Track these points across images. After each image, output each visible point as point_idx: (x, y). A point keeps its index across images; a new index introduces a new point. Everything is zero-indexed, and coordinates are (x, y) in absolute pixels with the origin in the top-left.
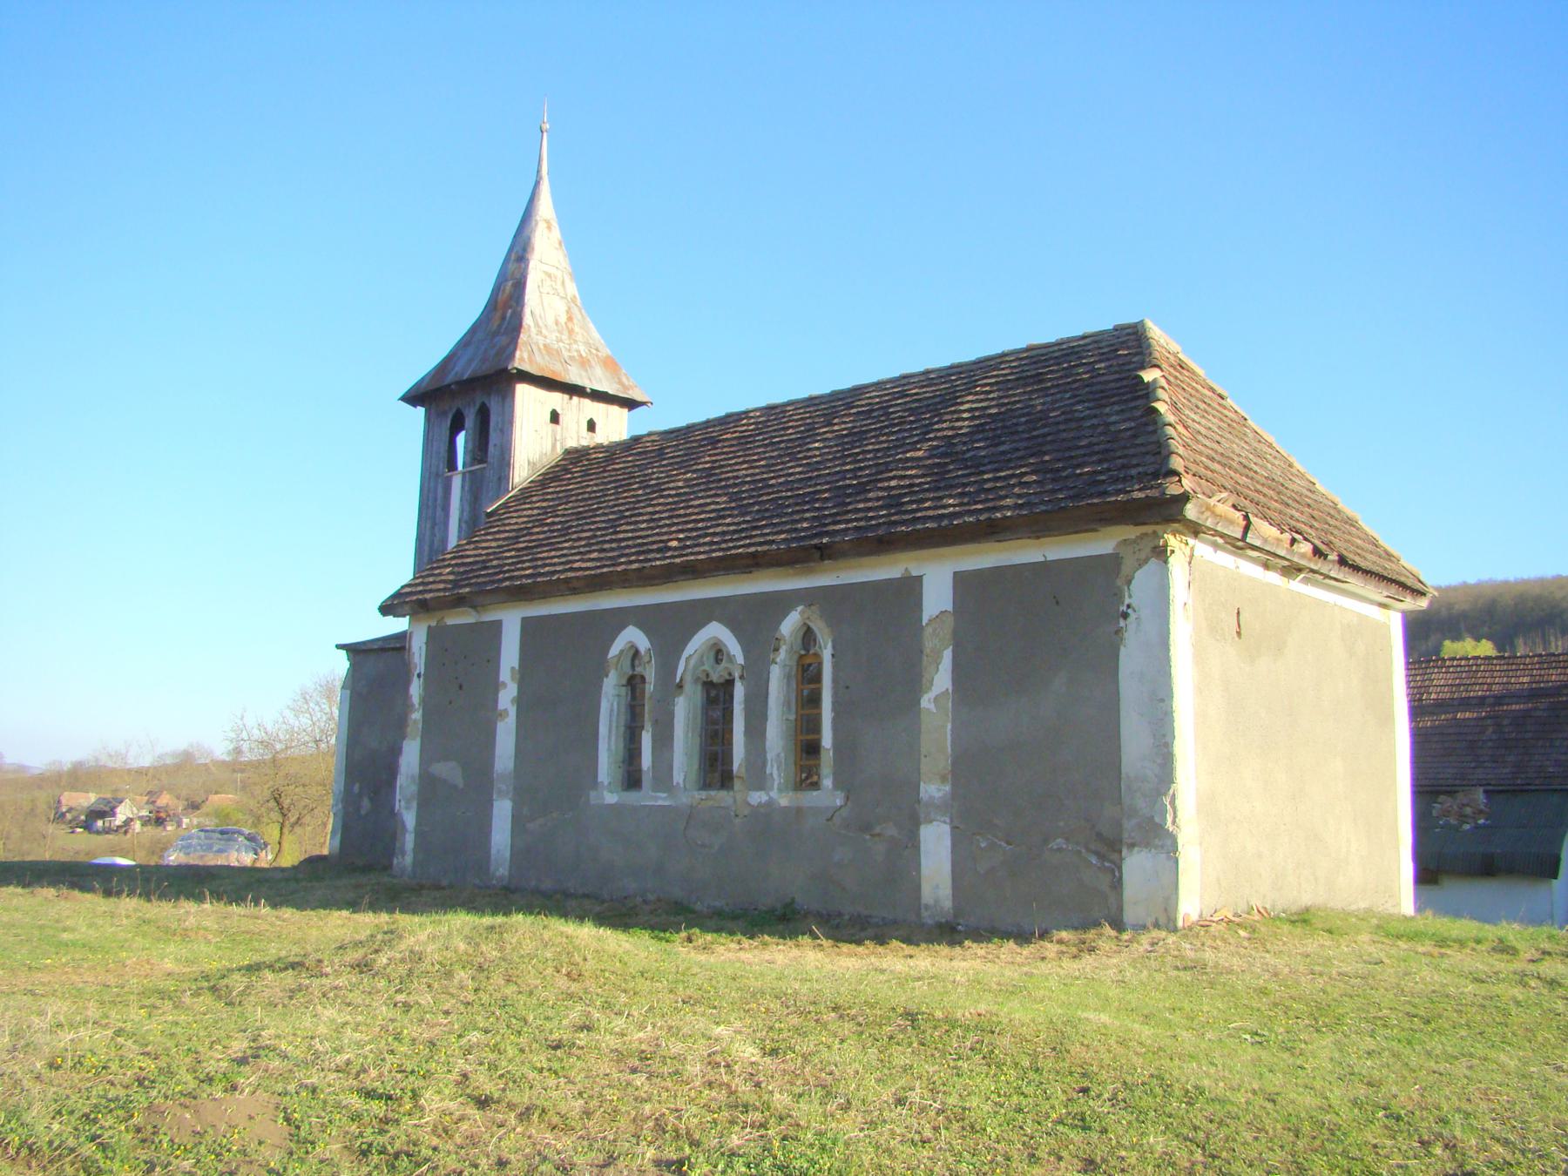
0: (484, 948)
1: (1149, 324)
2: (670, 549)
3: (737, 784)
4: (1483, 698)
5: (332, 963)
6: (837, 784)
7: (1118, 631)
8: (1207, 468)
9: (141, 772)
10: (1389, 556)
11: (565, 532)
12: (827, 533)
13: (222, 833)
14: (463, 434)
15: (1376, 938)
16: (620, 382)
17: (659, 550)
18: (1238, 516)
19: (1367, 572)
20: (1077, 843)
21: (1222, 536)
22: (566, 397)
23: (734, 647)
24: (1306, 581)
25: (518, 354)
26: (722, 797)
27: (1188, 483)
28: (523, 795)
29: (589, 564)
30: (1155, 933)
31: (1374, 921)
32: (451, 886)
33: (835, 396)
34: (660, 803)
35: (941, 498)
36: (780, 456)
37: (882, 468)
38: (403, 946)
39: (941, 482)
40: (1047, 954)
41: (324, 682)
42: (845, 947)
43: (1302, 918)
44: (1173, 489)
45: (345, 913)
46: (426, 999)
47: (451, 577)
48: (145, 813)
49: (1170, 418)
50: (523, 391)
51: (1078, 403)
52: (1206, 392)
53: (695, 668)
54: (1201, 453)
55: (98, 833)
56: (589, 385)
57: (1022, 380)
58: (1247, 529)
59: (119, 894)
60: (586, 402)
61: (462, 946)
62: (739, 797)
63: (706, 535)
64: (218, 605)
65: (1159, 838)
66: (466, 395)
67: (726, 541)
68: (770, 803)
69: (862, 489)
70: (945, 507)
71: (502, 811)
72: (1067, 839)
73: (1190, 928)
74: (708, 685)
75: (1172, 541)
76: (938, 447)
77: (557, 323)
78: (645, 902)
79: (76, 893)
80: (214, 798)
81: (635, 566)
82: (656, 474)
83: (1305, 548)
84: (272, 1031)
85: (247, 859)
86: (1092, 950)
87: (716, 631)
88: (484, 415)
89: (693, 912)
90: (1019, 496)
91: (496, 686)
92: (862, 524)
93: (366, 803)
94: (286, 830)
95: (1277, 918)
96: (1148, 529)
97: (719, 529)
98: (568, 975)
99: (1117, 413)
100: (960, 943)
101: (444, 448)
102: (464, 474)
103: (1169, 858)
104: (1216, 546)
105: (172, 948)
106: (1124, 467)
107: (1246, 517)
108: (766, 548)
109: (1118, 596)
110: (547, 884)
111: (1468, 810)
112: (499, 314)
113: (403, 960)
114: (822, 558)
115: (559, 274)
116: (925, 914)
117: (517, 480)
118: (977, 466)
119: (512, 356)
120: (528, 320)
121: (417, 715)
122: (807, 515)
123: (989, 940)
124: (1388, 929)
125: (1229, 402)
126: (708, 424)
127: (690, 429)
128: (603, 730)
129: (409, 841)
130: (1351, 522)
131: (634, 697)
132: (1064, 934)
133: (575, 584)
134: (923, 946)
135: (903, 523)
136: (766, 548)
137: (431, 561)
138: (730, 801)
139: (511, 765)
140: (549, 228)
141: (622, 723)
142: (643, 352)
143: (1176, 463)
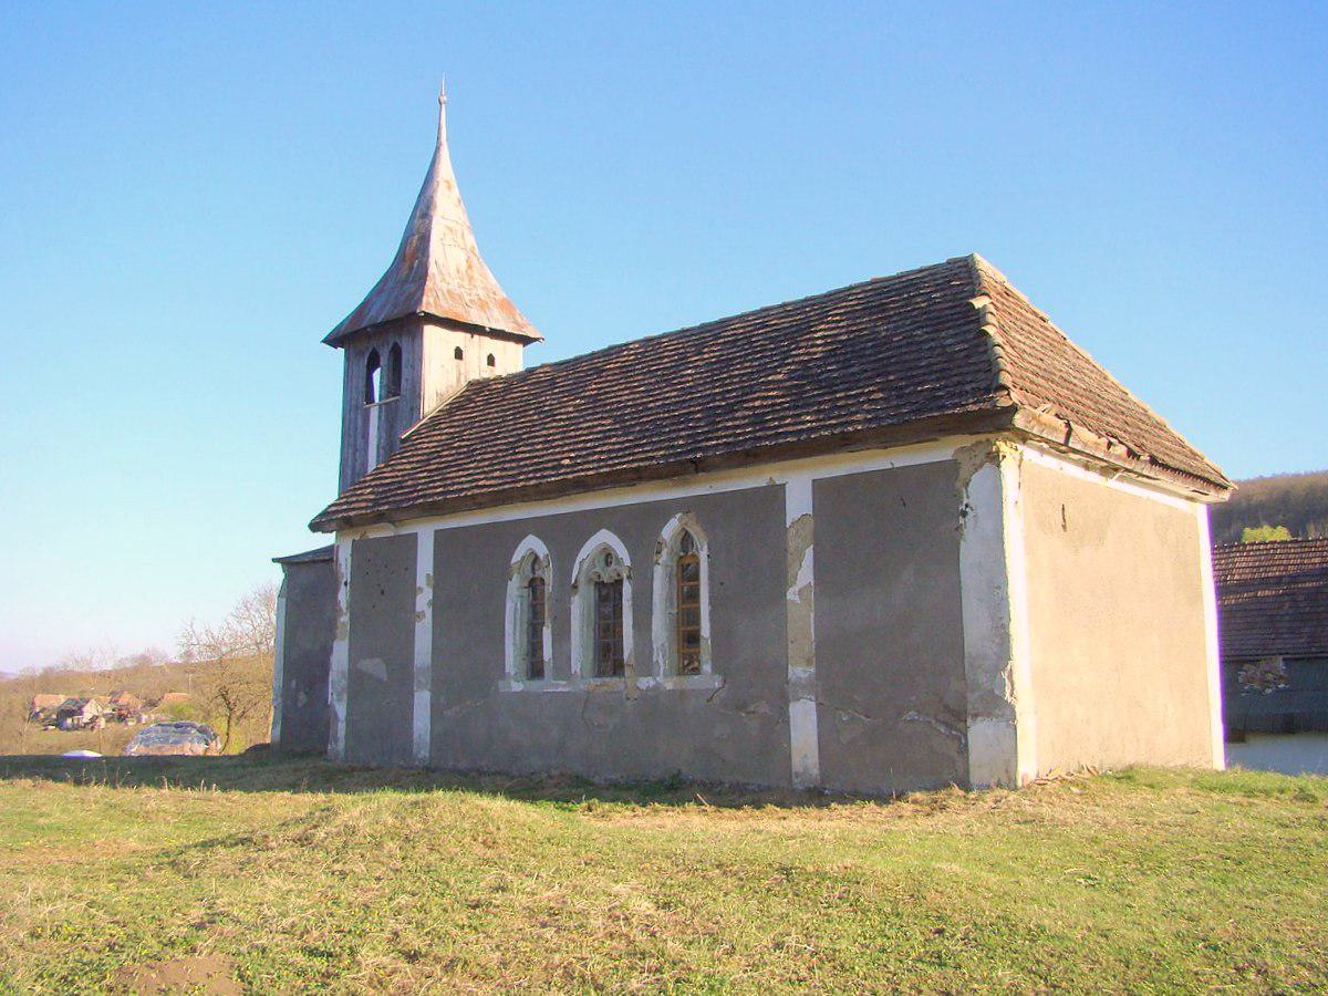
0: (409, 821)
1: (978, 257)
2: (563, 466)
3: (627, 671)
4: (1281, 577)
5: (277, 838)
6: (715, 670)
7: (959, 528)
8: (1032, 382)
9: (104, 675)
10: (1194, 455)
11: (470, 454)
12: (700, 449)
13: (177, 726)
14: (379, 369)
15: (1192, 791)
16: (516, 322)
17: (553, 468)
18: (1061, 423)
19: (1175, 470)
20: (927, 715)
21: (1047, 441)
22: (469, 335)
23: (622, 552)
24: (1121, 479)
25: (425, 299)
26: (614, 683)
27: (1016, 396)
28: (439, 685)
29: (493, 482)
30: (998, 792)
31: (1190, 776)
32: (379, 768)
33: (704, 328)
34: (560, 690)
35: (799, 415)
36: (658, 382)
37: (747, 390)
38: (338, 822)
39: (799, 402)
40: (903, 813)
41: (262, 592)
42: (727, 812)
43: (1127, 776)
44: (1003, 402)
45: (286, 794)
46: (360, 868)
47: (372, 497)
48: (108, 711)
49: (999, 339)
50: (430, 331)
51: (918, 328)
52: (1029, 315)
53: (588, 570)
54: (1026, 370)
55: (68, 729)
56: (488, 325)
57: (867, 310)
58: (1068, 435)
59: (87, 783)
60: (486, 339)
61: (390, 821)
62: (629, 682)
63: (595, 453)
64: (174, 532)
65: (999, 708)
66: (381, 336)
67: (612, 459)
68: (657, 688)
69: (730, 409)
70: (803, 423)
71: (422, 700)
72: (918, 712)
73: (1029, 787)
74: (600, 585)
75: (1004, 447)
76: (796, 370)
77: (458, 272)
78: (550, 777)
79: (50, 783)
80: (169, 696)
81: (532, 482)
82: (549, 401)
83: (1120, 450)
84: (226, 899)
85: (200, 749)
86: (943, 808)
87: (605, 537)
88: (396, 353)
89: (592, 784)
90: (868, 412)
91: (414, 590)
92: (731, 440)
93: (302, 698)
94: (232, 723)
95: (1105, 775)
96: (982, 437)
97: (605, 448)
98: (484, 842)
99: (952, 336)
100: (827, 806)
101: (362, 383)
102: (380, 406)
103: (1008, 726)
104: (1042, 450)
105: (136, 828)
106: (959, 383)
107: (1068, 425)
108: (647, 463)
109: (957, 497)
110: (463, 765)
111: (1270, 677)
112: (407, 265)
113: (338, 834)
114: (697, 471)
115: (458, 228)
116: (796, 781)
117: (426, 410)
118: (830, 387)
119: (420, 301)
120: (432, 269)
121: (345, 619)
122: (683, 433)
123: (853, 802)
124: (1203, 783)
125: (1050, 324)
126: (593, 356)
127: (578, 360)
128: (509, 627)
129: (341, 729)
130: (1160, 426)
131: (535, 598)
132: (918, 795)
133: (480, 499)
134: (795, 809)
135: (767, 438)
136: (647, 463)
137: (353, 483)
138: (622, 687)
139: (429, 660)
140: (449, 188)
141: (525, 618)
142: (529, 297)
143: (1005, 379)
